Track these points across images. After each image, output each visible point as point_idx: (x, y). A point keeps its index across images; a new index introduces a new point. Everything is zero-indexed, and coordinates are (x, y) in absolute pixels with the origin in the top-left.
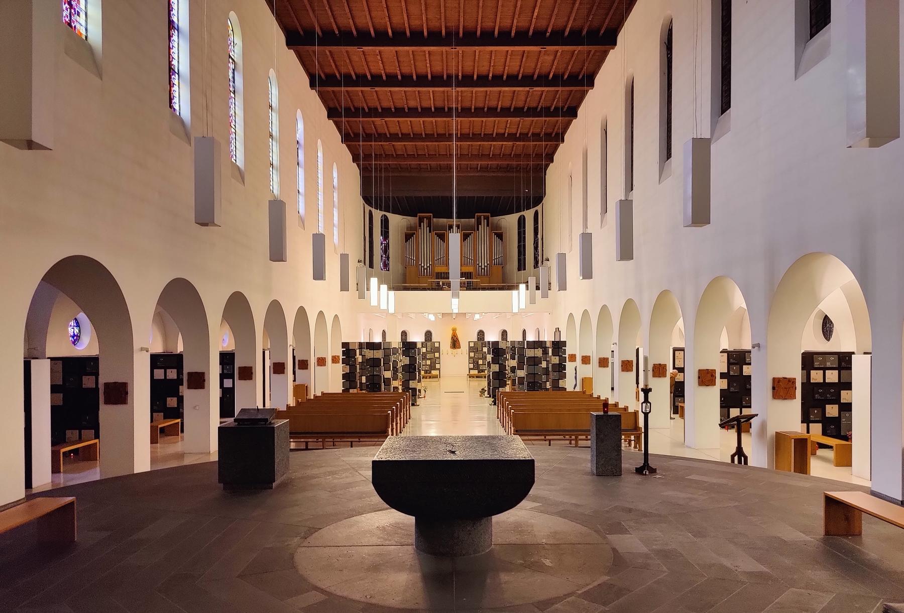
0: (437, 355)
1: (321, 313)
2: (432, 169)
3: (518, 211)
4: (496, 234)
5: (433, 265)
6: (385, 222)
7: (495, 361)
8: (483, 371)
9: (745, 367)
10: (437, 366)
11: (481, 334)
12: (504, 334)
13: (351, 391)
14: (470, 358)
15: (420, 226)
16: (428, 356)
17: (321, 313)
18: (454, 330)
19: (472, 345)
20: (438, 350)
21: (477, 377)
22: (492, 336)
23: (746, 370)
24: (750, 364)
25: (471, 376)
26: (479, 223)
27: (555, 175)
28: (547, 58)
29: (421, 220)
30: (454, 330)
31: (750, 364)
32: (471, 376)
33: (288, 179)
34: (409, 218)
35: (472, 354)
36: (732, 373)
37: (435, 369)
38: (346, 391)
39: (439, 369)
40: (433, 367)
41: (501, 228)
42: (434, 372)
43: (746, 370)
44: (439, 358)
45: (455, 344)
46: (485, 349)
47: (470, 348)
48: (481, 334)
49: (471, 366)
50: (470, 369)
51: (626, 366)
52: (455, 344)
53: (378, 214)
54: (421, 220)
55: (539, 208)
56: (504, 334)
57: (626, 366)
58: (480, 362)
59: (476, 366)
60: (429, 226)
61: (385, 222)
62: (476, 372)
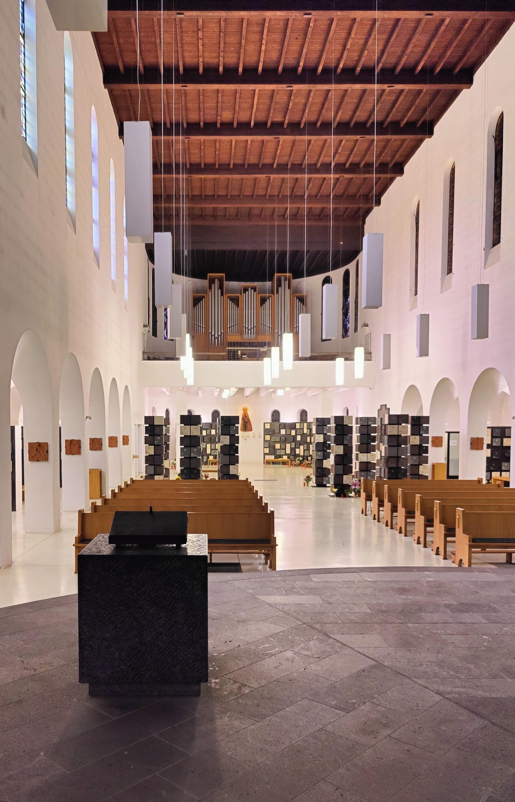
1: (114, 379)
2: (237, 216)
3: (343, 265)
4: (298, 298)
5: (225, 334)
8: (280, 456)
9: (505, 440)
11: (276, 415)
12: (304, 414)
13: (157, 478)
14: (265, 441)
15: (210, 288)
17: (114, 379)
19: (268, 426)
21: (274, 463)
22: (289, 417)
23: (506, 442)
24: (510, 437)
25: (268, 463)
26: (279, 285)
27: (385, 222)
28: (376, 97)
29: (212, 281)
31: (510, 437)
32: (268, 463)
33: (83, 197)
34: (196, 280)
35: (268, 437)
36: (494, 444)
38: (150, 477)
41: (301, 292)
43: (506, 442)
48: (276, 415)
49: (267, 451)
50: (265, 454)
54: (212, 281)
55: (351, 266)
56: (304, 414)
58: (278, 446)
59: (273, 451)
60: (221, 287)
62: (272, 458)
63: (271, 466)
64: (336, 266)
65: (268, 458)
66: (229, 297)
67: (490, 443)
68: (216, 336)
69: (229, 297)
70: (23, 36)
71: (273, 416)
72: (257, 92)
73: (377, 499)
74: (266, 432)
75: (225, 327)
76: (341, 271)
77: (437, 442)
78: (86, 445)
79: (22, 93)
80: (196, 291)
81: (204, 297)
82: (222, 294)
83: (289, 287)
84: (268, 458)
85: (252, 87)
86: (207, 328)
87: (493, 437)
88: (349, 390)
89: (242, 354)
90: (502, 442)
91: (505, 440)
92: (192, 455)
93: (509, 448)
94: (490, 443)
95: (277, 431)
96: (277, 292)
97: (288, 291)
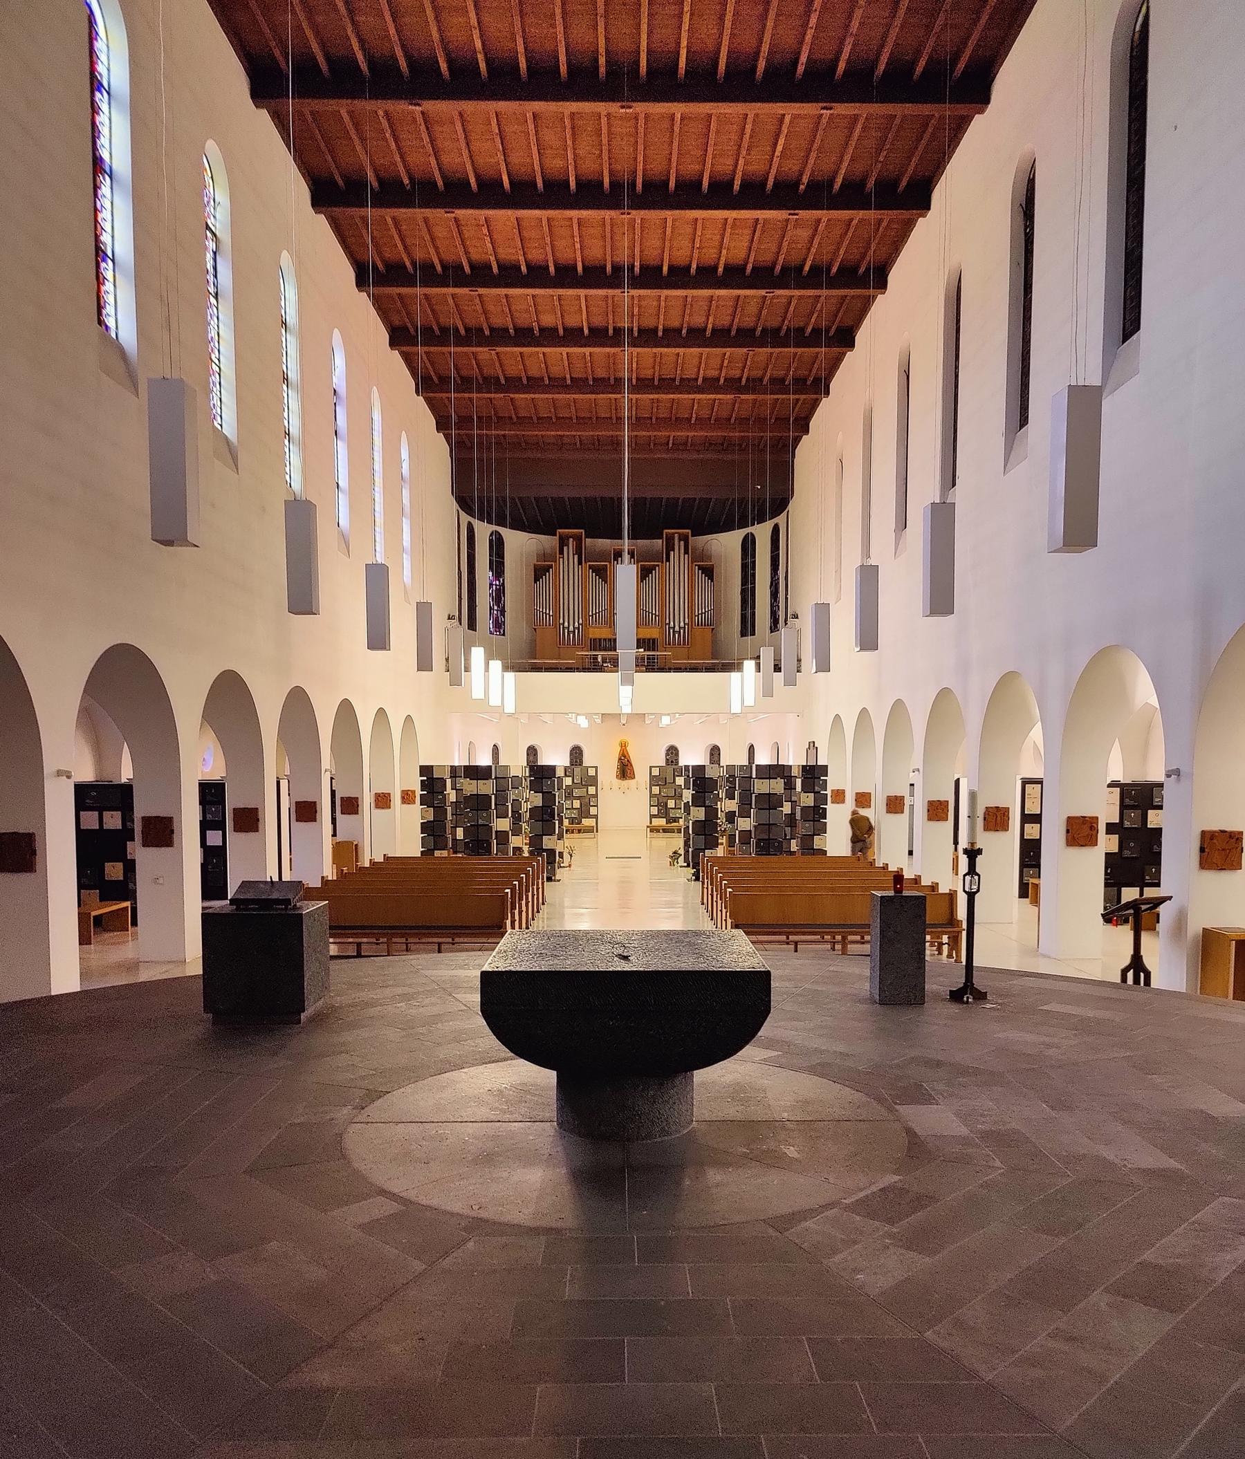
0: (592, 790)
3: (743, 525)
6: (497, 546)
7: (698, 801)
8: (676, 820)
9: (1151, 814)
10: (593, 811)
11: (672, 752)
12: (715, 752)
14: (651, 796)
15: (561, 552)
16: (576, 793)
18: (623, 746)
19: (656, 772)
20: (593, 781)
21: (665, 831)
23: (1154, 819)
24: (1161, 807)
25: (654, 830)
30: (623, 746)
35: (656, 790)
36: (1127, 824)
37: (588, 816)
39: (596, 817)
40: (584, 812)
41: (709, 558)
42: (586, 822)
43: (1154, 819)
44: (596, 796)
45: (625, 770)
46: (680, 781)
47: (652, 777)
48: (672, 752)
49: (655, 811)
50: (652, 816)
51: (936, 811)
52: (625, 770)
53: (484, 531)
54: (563, 542)
55: (780, 520)
56: (715, 752)
57: (936, 811)
58: (671, 804)
59: (664, 811)
60: (578, 551)
61: (497, 546)
62: (661, 822)
63: (661, 834)
64: (761, 520)
65: (656, 822)
66: (590, 567)
67: (1116, 819)
68: (571, 628)
69: (590, 567)
70: (216, 297)
71: (667, 754)
72: (787, 119)
73: (959, 918)
74: (654, 781)
75: (586, 616)
76: (768, 526)
77: (839, 796)
78: (396, 799)
79: (216, 368)
80: (543, 556)
81: (551, 567)
82: (580, 563)
83: (686, 552)
84: (656, 822)
85: (778, 108)
86: (556, 615)
87: (1123, 807)
88: (728, 715)
89: (604, 661)
90: (1145, 818)
91: (1151, 814)
92: (480, 822)
93: (1158, 832)
94: (1116, 819)
95: (669, 780)
96: (668, 560)
97: (685, 559)
